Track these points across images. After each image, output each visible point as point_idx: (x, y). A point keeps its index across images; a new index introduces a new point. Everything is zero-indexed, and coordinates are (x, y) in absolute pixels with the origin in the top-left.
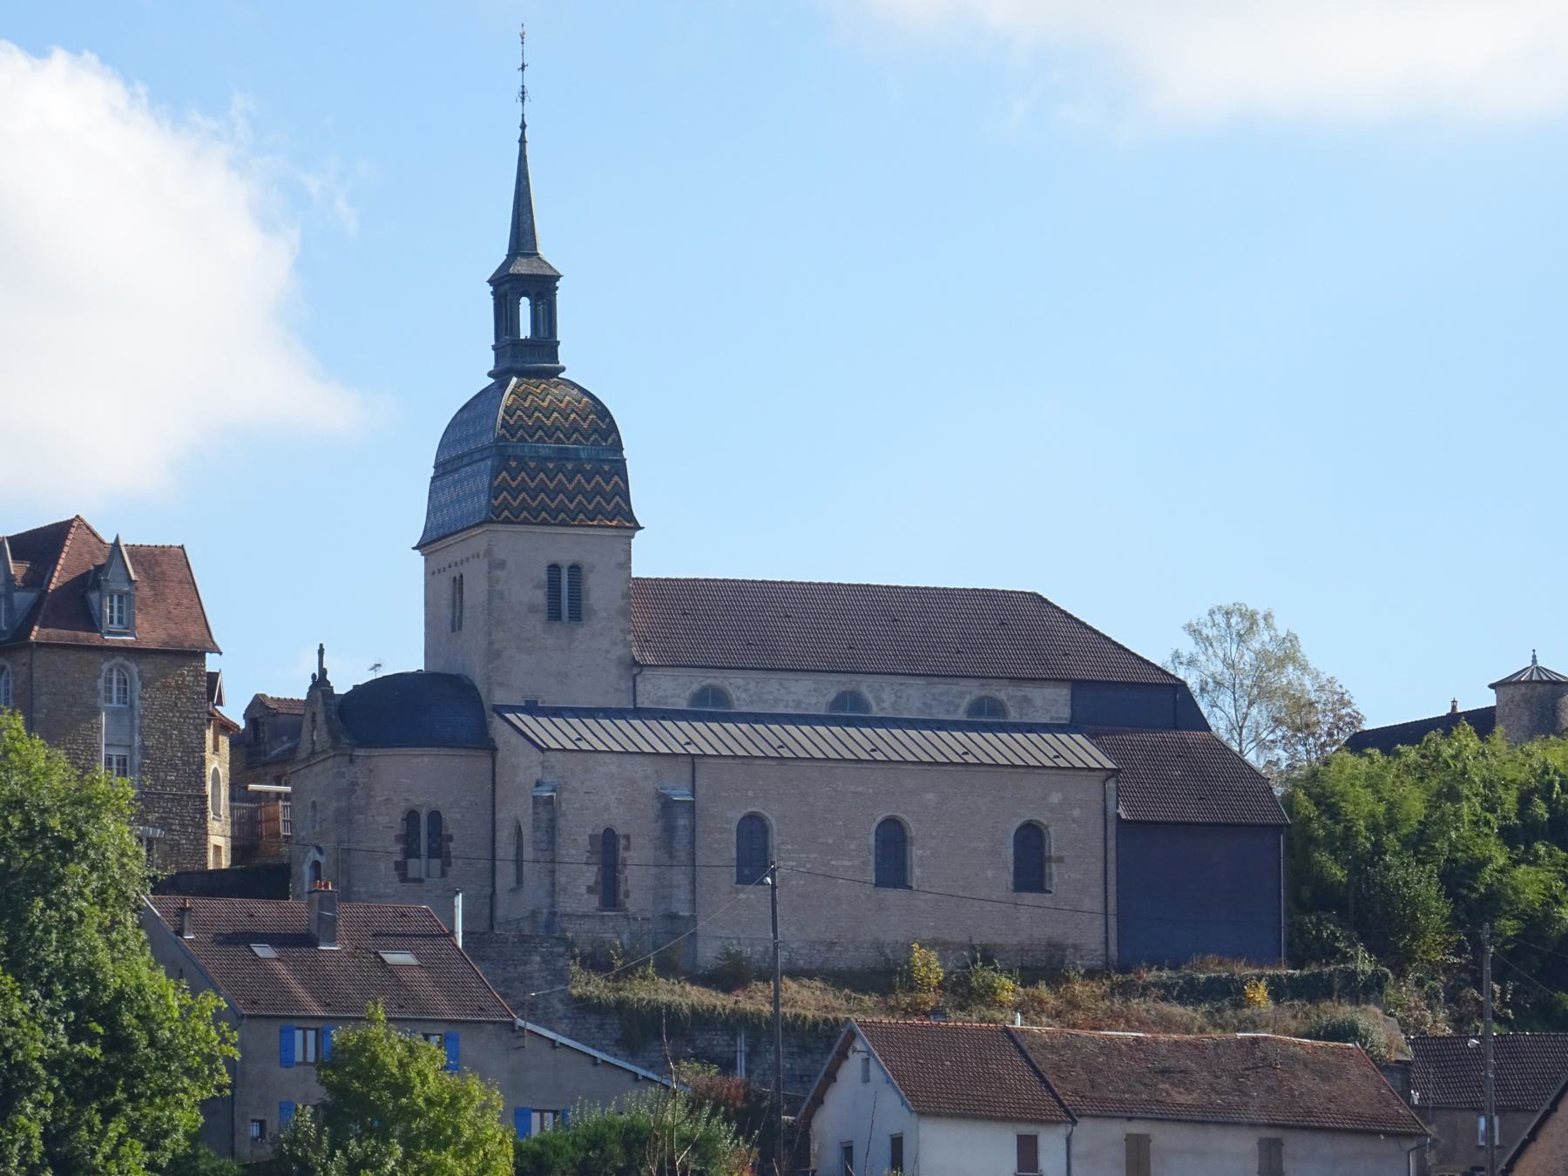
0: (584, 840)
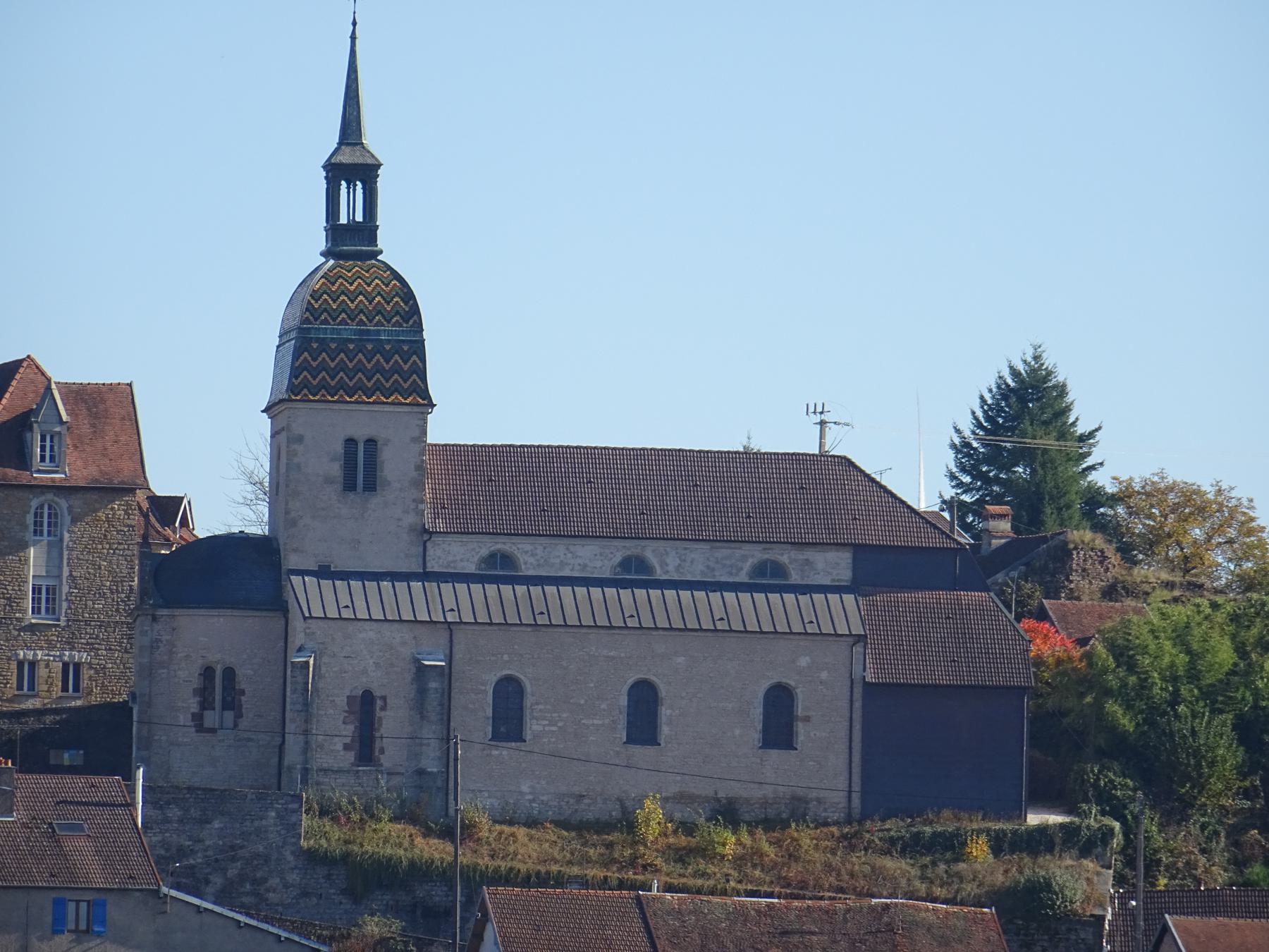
0: (342, 701)
